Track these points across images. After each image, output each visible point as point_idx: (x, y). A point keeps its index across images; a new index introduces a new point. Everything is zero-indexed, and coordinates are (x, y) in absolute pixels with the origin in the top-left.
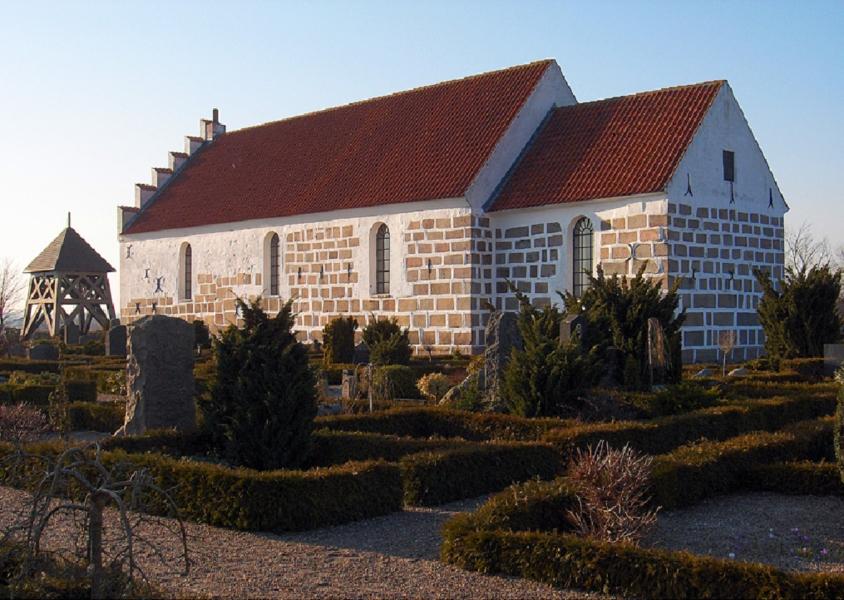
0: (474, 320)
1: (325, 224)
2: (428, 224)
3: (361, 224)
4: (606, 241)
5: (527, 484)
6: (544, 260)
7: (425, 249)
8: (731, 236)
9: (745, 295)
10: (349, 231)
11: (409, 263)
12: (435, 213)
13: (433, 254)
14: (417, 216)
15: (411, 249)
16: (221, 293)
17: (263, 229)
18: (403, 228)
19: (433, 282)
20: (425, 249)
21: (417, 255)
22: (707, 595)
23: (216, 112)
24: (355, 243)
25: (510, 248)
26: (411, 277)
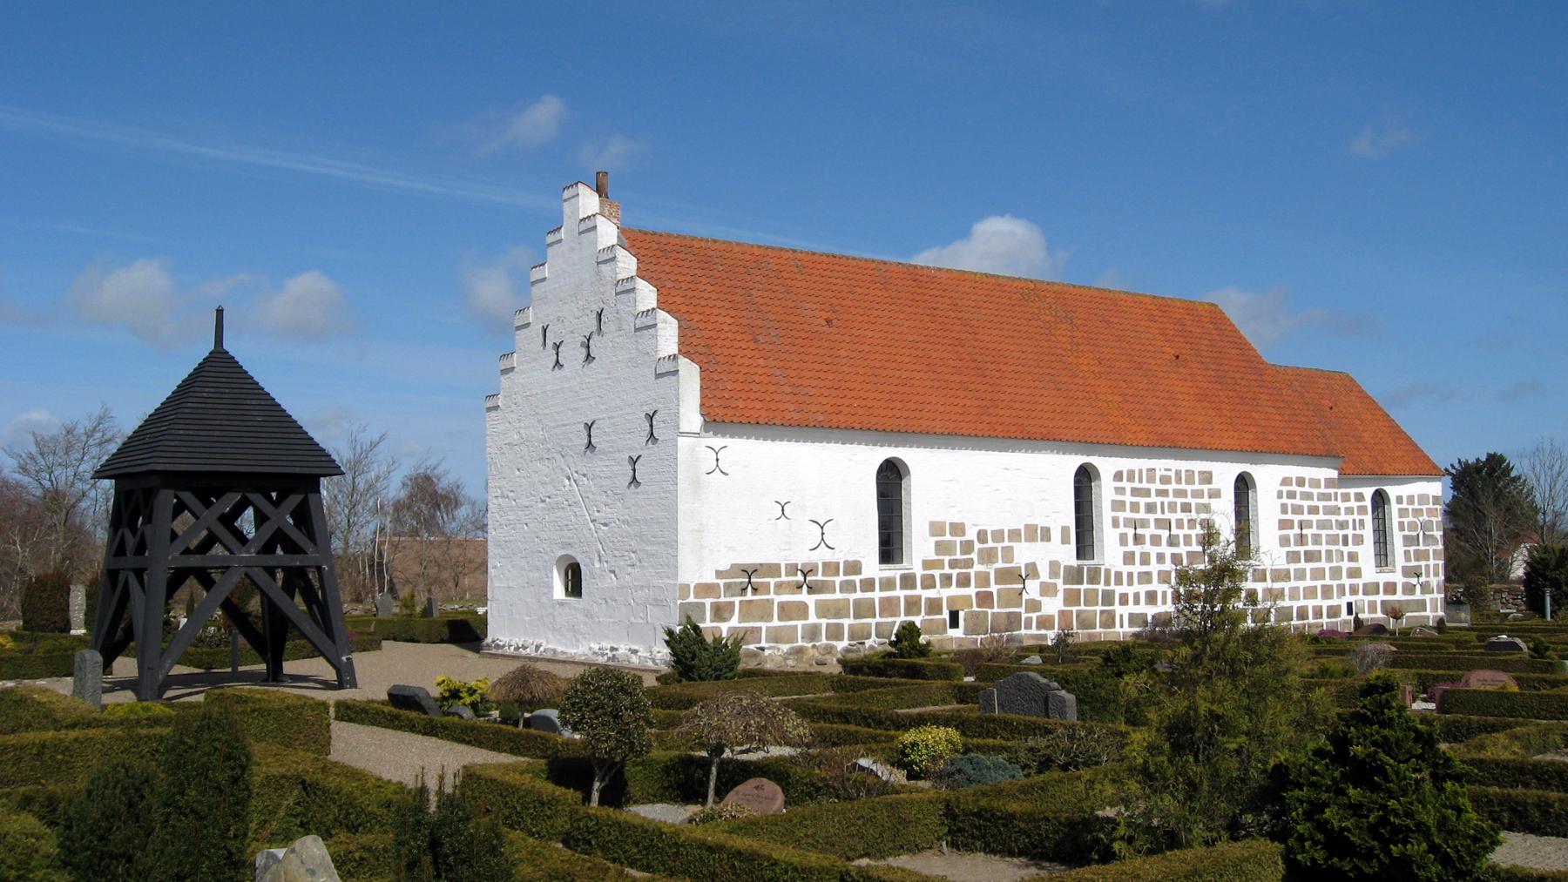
0: (1177, 597)
1: (1183, 465)
2: (1301, 482)
3: (1225, 473)
4: (1176, 542)
5: (1435, 736)
6: (1354, 529)
7: (1298, 510)
8: (972, 567)
9: (1112, 587)
10: (1207, 478)
11: (1284, 524)
12: (1309, 472)
13: (1306, 516)
14: (1294, 471)
15: (1284, 509)
16: (988, 556)
17: (1073, 457)
18: (1276, 486)
19: (1306, 548)
20: (1298, 510)
21: (1289, 516)
22: (184, 621)
23: (655, 412)
24: (1215, 494)
25: (1318, 521)
26: (1284, 541)
